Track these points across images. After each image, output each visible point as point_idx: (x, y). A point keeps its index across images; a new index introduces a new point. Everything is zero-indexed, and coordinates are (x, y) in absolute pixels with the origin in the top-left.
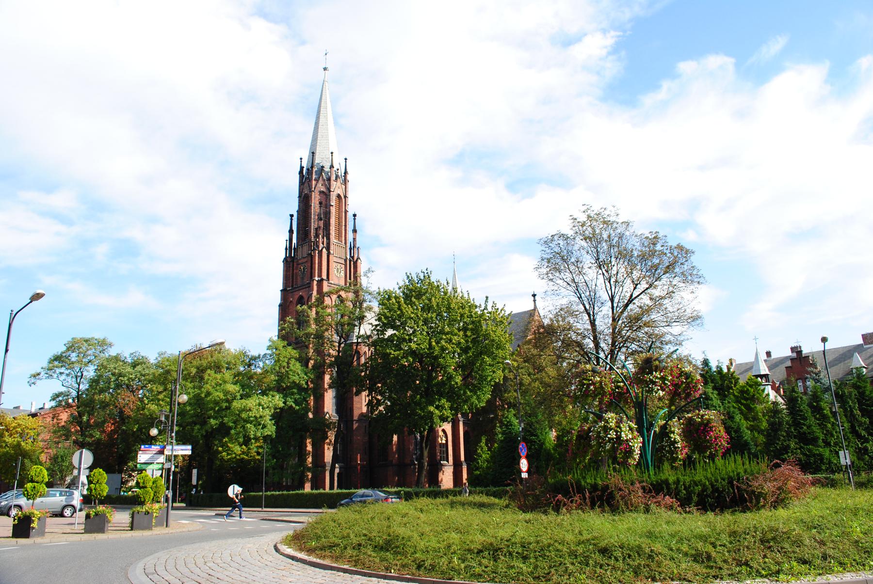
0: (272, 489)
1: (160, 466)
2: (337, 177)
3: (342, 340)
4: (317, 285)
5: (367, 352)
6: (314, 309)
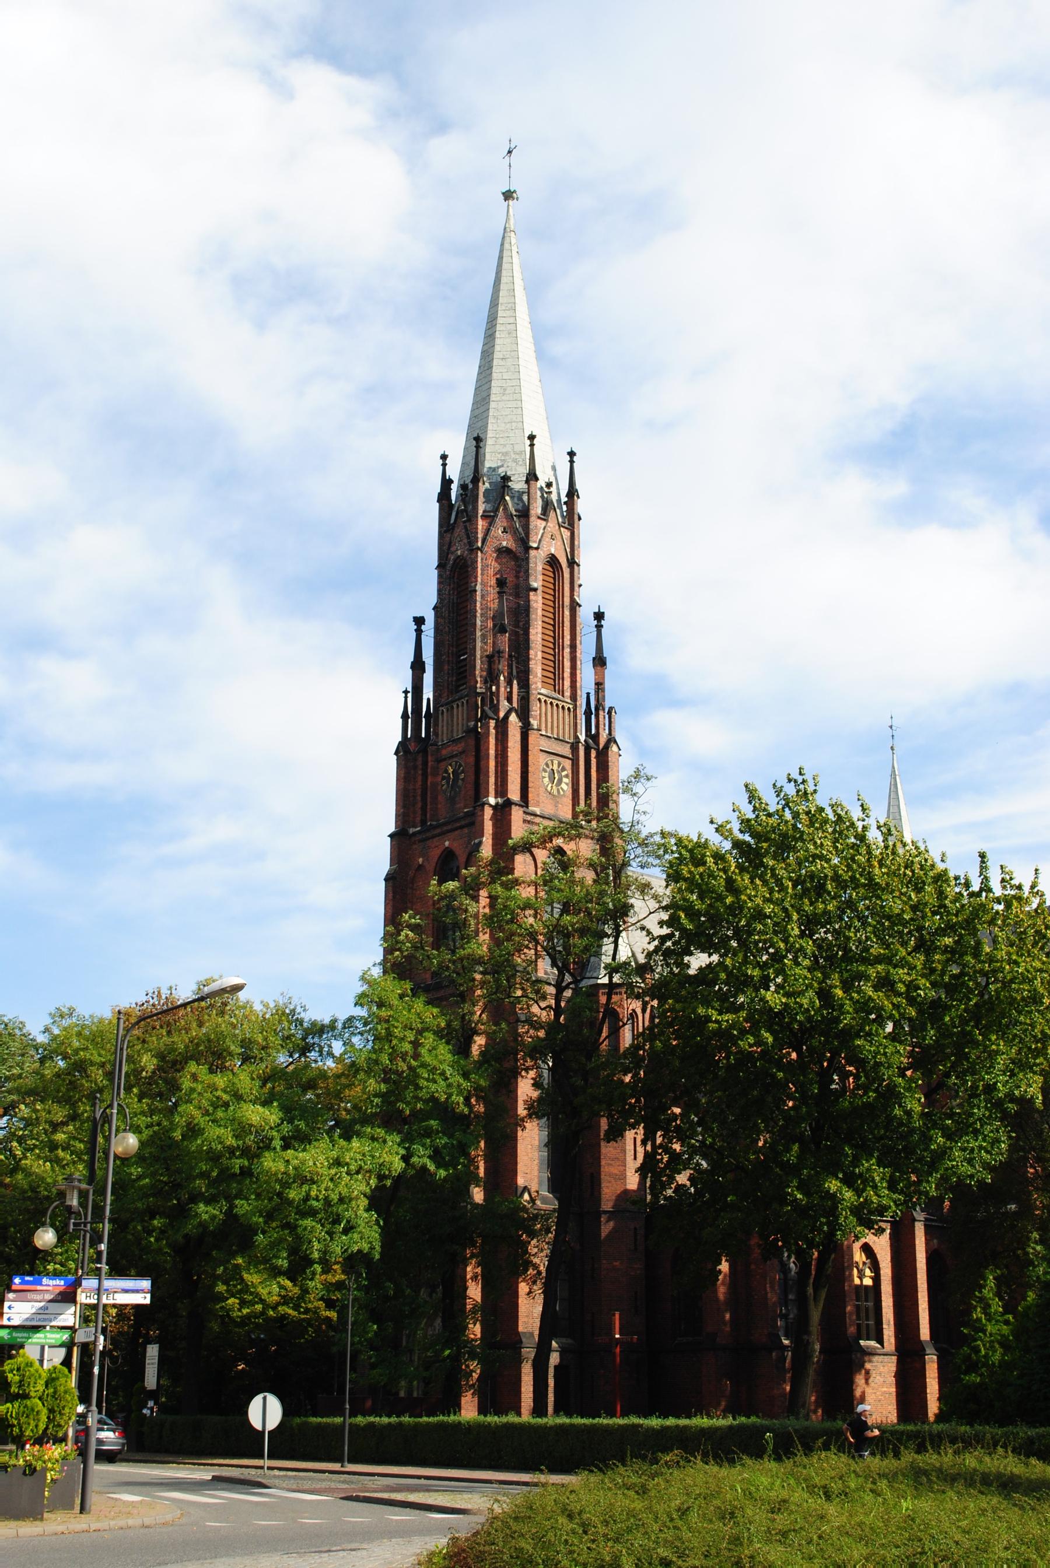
0: (369, 1403)
1: (65, 1336)
2: (547, 506)
3: (568, 978)
4: (494, 818)
5: (639, 1011)
6: (483, 893)
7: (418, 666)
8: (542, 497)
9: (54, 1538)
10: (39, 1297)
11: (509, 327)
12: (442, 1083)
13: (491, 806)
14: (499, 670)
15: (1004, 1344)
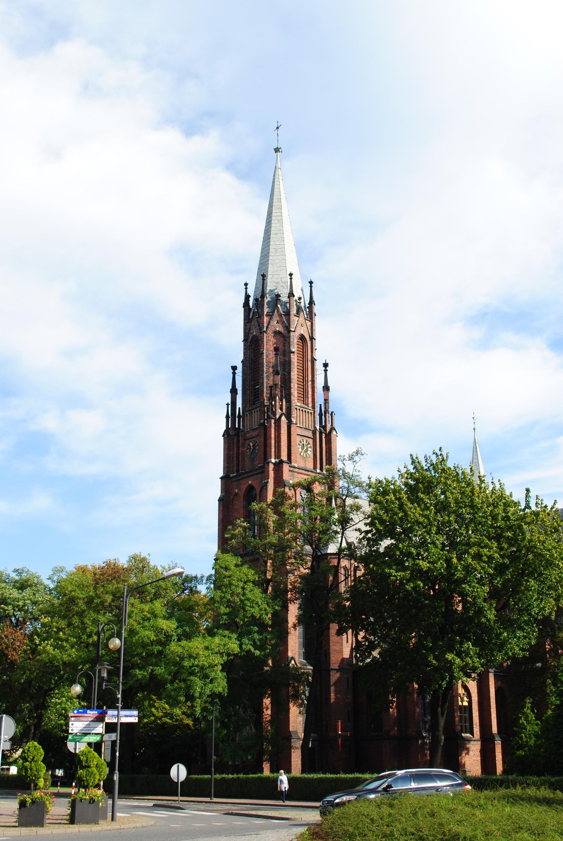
2: (299, 309)
4: (274, 469)
7: (234, 391)
8: (296, 305)
9: (106, 832)
10: (86, 719)
11: (278, 218)
12: (257, 608)
13: (272, 463)
14: (276, 394)
15: (537, 736)
